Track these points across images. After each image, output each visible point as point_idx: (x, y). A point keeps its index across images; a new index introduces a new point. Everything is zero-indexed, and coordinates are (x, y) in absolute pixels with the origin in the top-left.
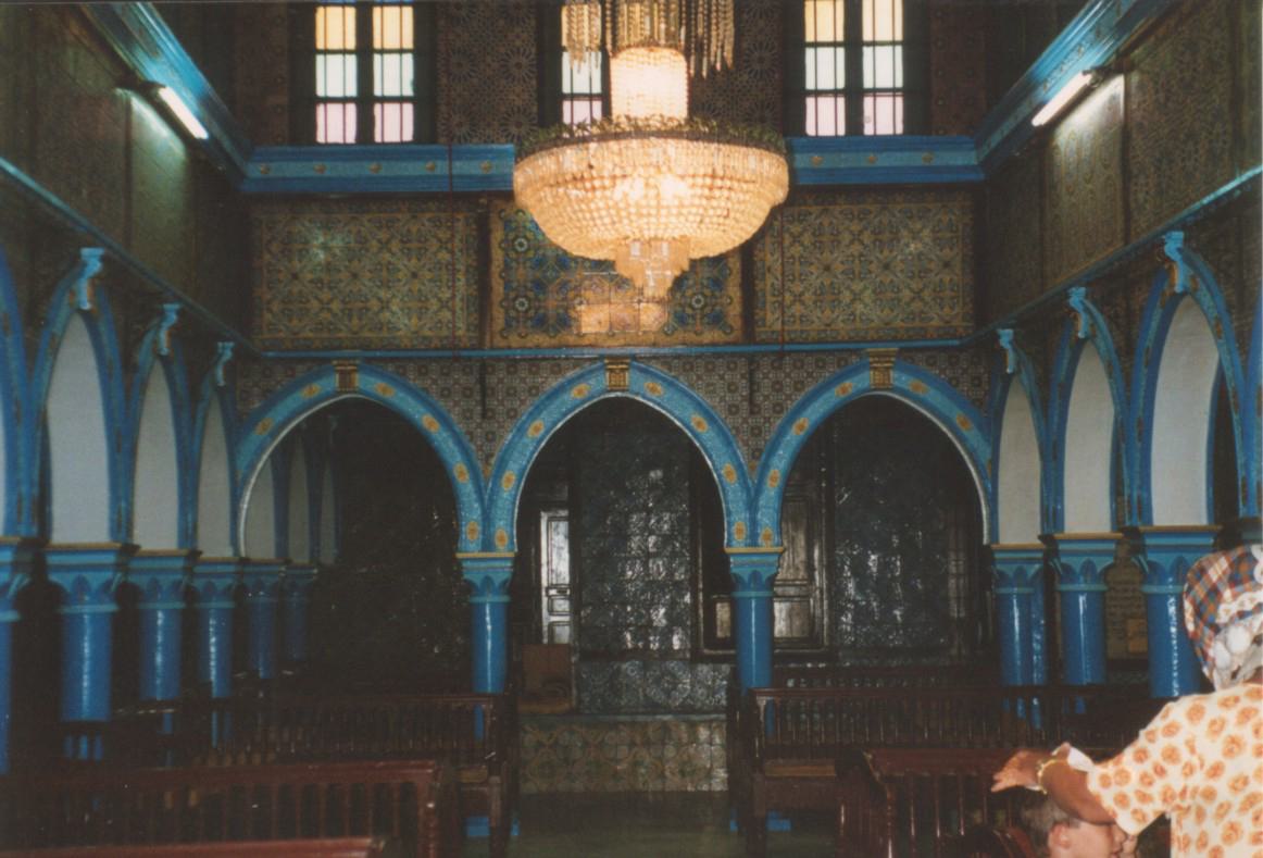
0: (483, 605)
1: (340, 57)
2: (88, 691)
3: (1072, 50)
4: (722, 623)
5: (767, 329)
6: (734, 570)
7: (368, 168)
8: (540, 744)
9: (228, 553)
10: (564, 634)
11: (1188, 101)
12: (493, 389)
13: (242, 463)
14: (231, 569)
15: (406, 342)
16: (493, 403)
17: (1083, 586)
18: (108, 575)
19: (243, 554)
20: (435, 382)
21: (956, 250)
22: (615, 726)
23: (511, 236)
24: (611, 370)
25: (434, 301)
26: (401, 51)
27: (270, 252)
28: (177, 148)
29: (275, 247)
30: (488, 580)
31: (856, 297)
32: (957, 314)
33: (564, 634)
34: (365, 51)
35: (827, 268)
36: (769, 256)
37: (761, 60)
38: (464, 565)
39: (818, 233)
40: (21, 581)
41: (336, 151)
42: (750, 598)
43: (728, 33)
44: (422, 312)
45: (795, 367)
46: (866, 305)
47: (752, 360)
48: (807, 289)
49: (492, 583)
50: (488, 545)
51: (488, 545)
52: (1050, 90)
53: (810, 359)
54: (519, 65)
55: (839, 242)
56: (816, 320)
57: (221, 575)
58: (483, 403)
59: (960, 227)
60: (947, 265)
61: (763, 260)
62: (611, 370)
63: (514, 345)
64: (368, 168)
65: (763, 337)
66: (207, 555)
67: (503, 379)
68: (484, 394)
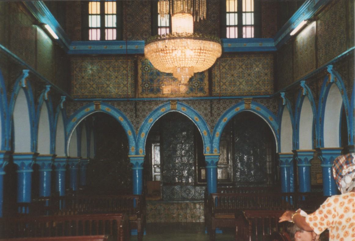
0: (136, 170)
1: (96, 16)
2: (25, 194)
3: (301, 14)
4: (203, 175)
5: (216, 92)
6: (206, 160)
7: (103, 47)
8: (152, 209)
9: (64, 155)
10: (159, 178)
11: (334, 28)
12: (138, 109)
13: (68, 130)
14: (65, 160)
15: (114, 96)
16: (138, 113)
17: (304, 165)
18: (30, 162)
19: (68, 156)
20: (122, 107)
21: (269, 70)
22: (173, 204)
23: (144, 66)
24: (172, 104)
25: (122, 85)
26: (113, 14)
27: (76, 71)
28: (50, 41)
29: (77, 70)
30: (137, 163)
31: (241, 84)
32: (269, 88)
33: (159, 178)
34: (103, 14)
35: (233, 75)
36: (216, 72)
37: (214, 17)
38: (131, 159)
39: (230, 65)
41: (95, 43)
42: (211, 168)
43: (204, 9)
46: (243, 86)
48: (227, 81)
49: (138, 164)
50: (137, 153)
51: (137, 153)
52: (295, 25)
53: (228, 101)
54: (146, 18)
55: (236, 68)
57: (62, 162)
58: (136, 113)
59: (270, 64)
60: (266, 74)
61: (214, 73)
62: (172, 104)
63: (144, 97)
64: (103, 47)
65: (215, 95)
66: (58, 156)
67: (141, 106)
68: (136, 111)
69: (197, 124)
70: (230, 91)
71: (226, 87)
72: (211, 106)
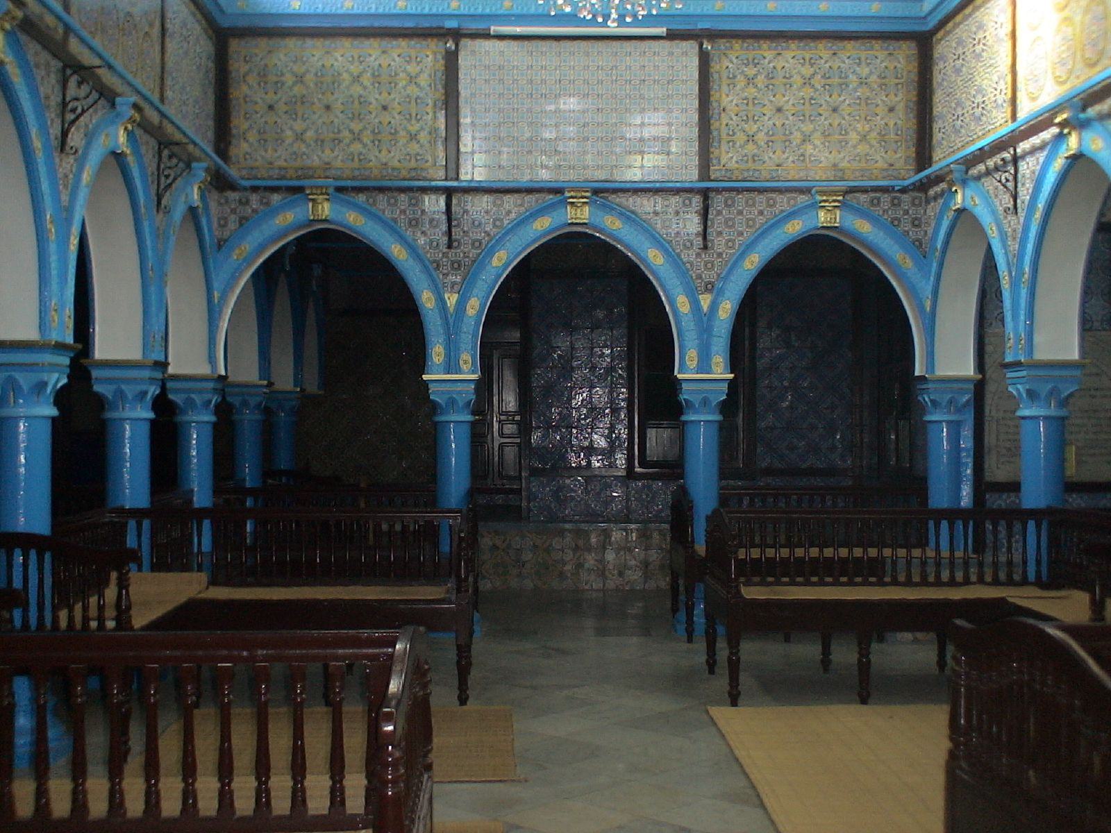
0: (16, 419)
5: (721, 167)
8: (495, 547)
9: (204, 369)
13: (217, 286)
15: (376, 172)
18: (207, 397)
21: (900, 96)
22: (561, 533)
25: (289, 133)
29: (252, 80)
30: (452, 402)
31: (806, 139)
32: (901, 158)
39: (770, 77)
40: (155, 391)
44: (843, 144)
45: (914, 204)
47: (705, 194)
49: (710, 402)
56: (373, 158)
57: (200, 391)
59: (905, 74)
60: (891, 110)
61: (719, 102)
65: (718, 174)
69: (630, 251)
70: (788, 55)
71: (743, 71)
72: (705, 214)
